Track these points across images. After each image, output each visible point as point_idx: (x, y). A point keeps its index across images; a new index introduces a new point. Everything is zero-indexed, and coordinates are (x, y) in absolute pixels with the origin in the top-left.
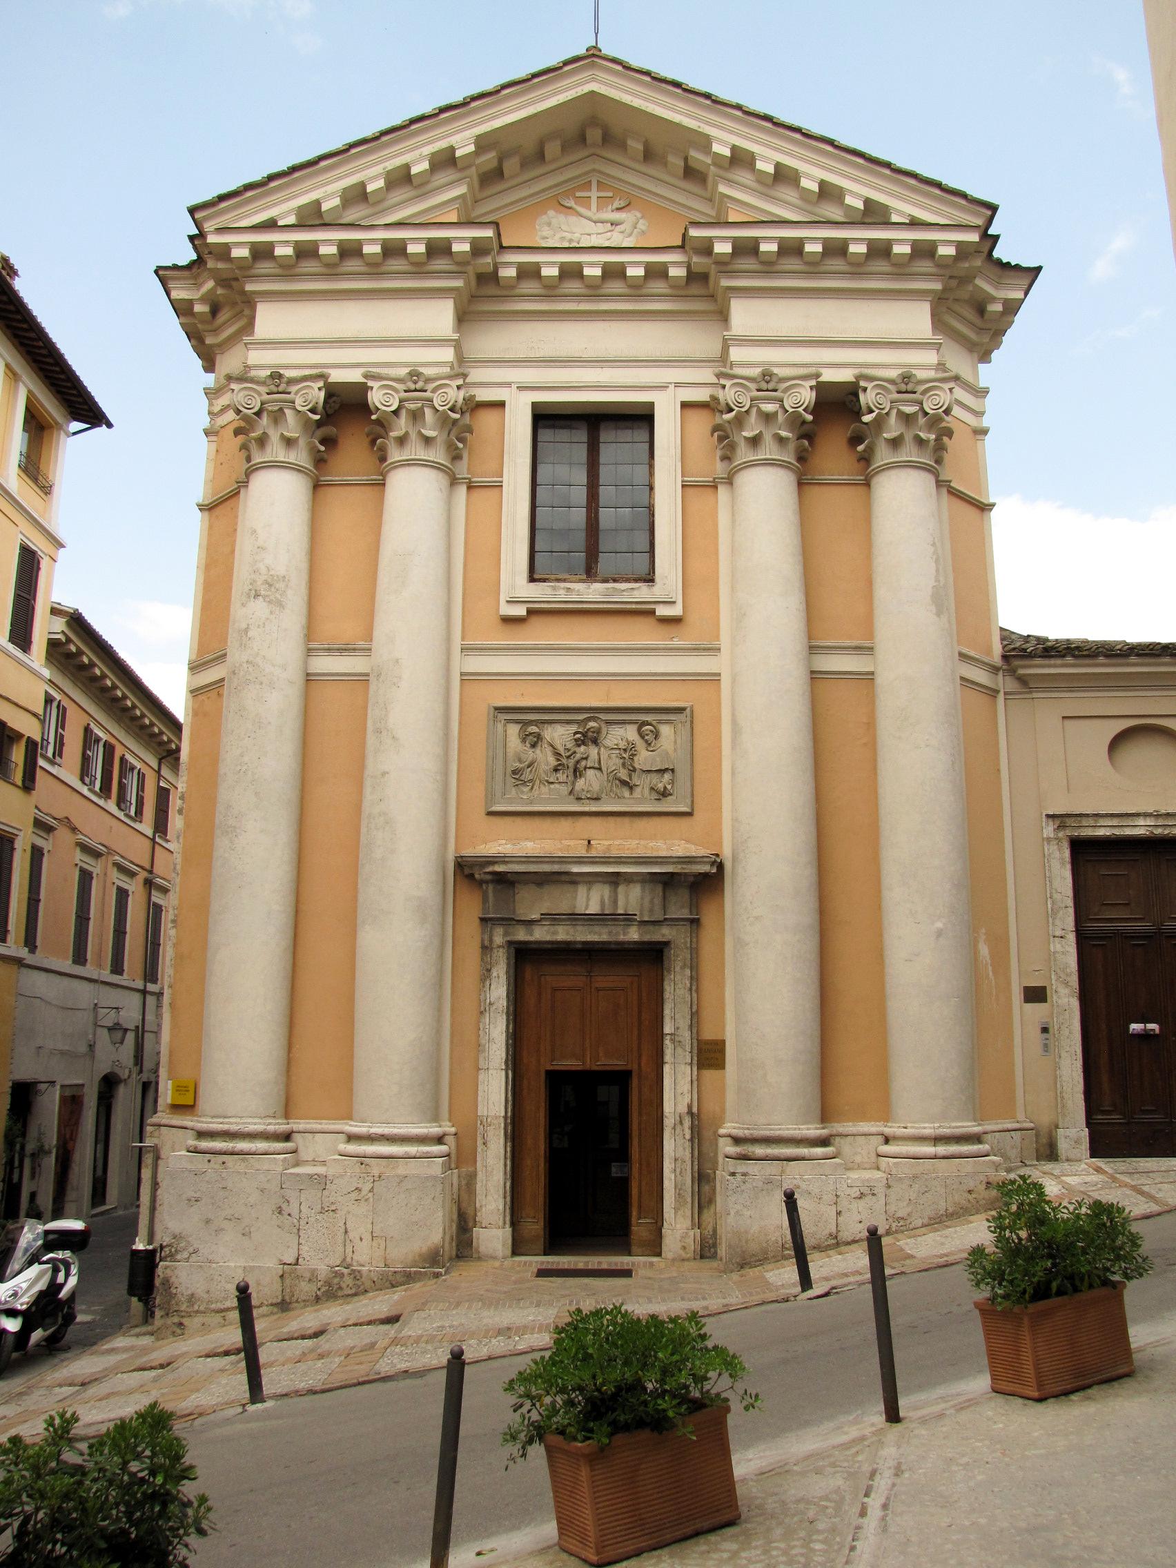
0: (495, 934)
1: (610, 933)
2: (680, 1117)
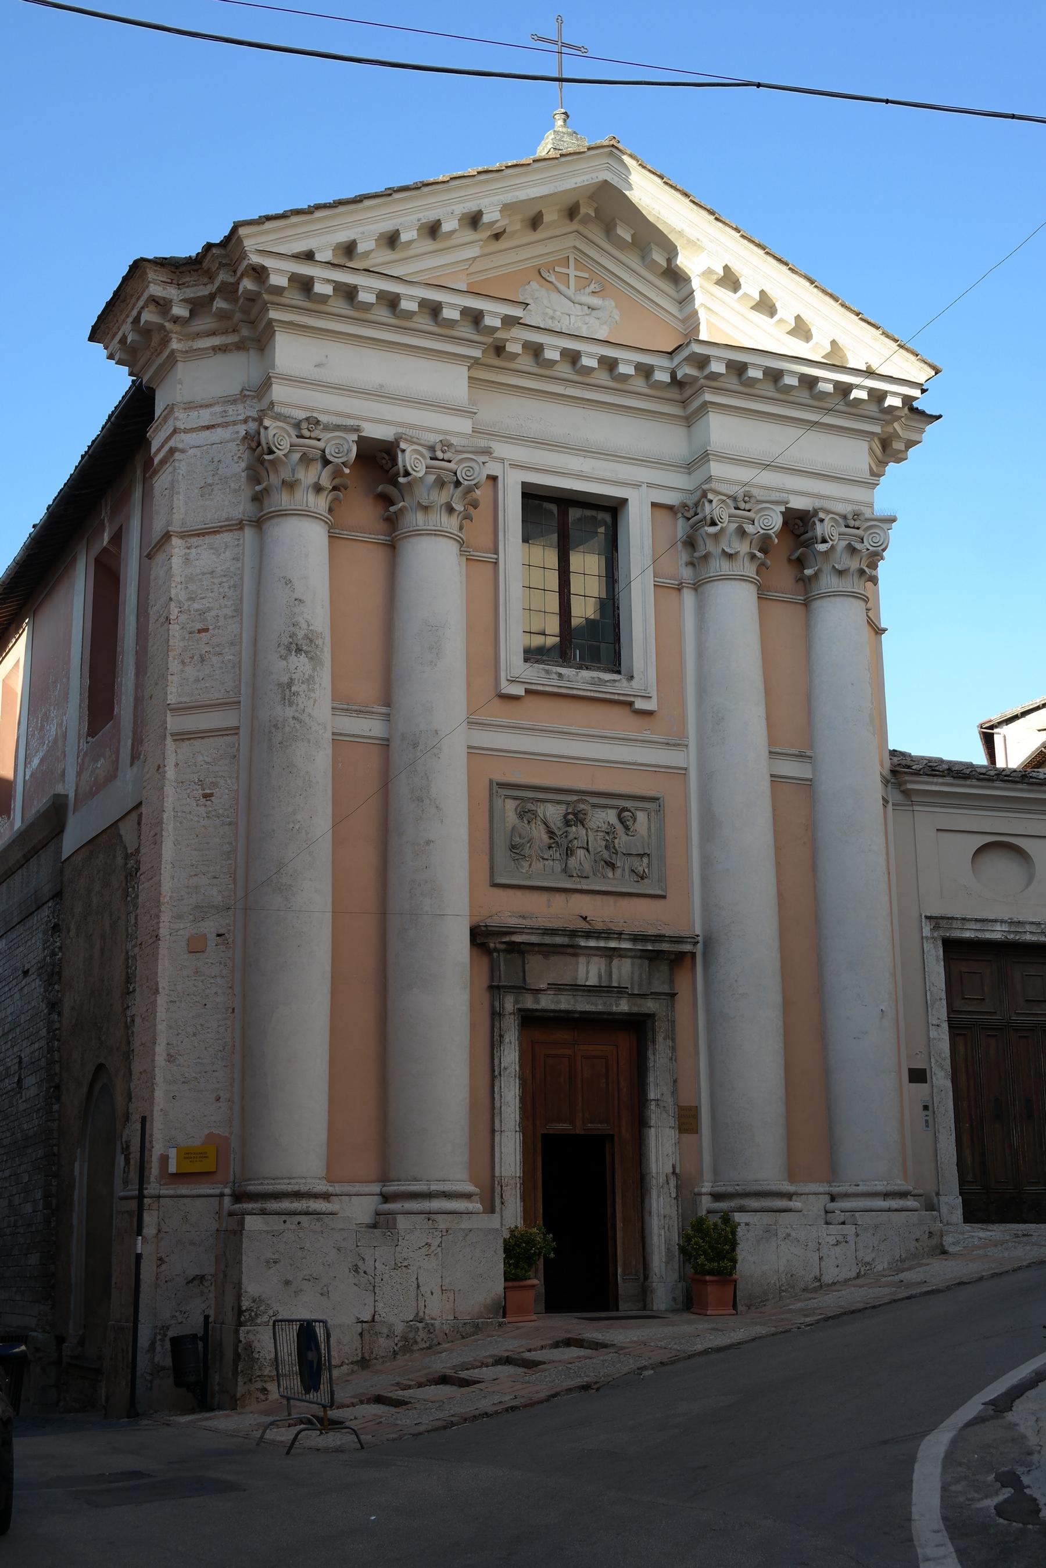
0: (506, 1001)
1: (605, 1004)
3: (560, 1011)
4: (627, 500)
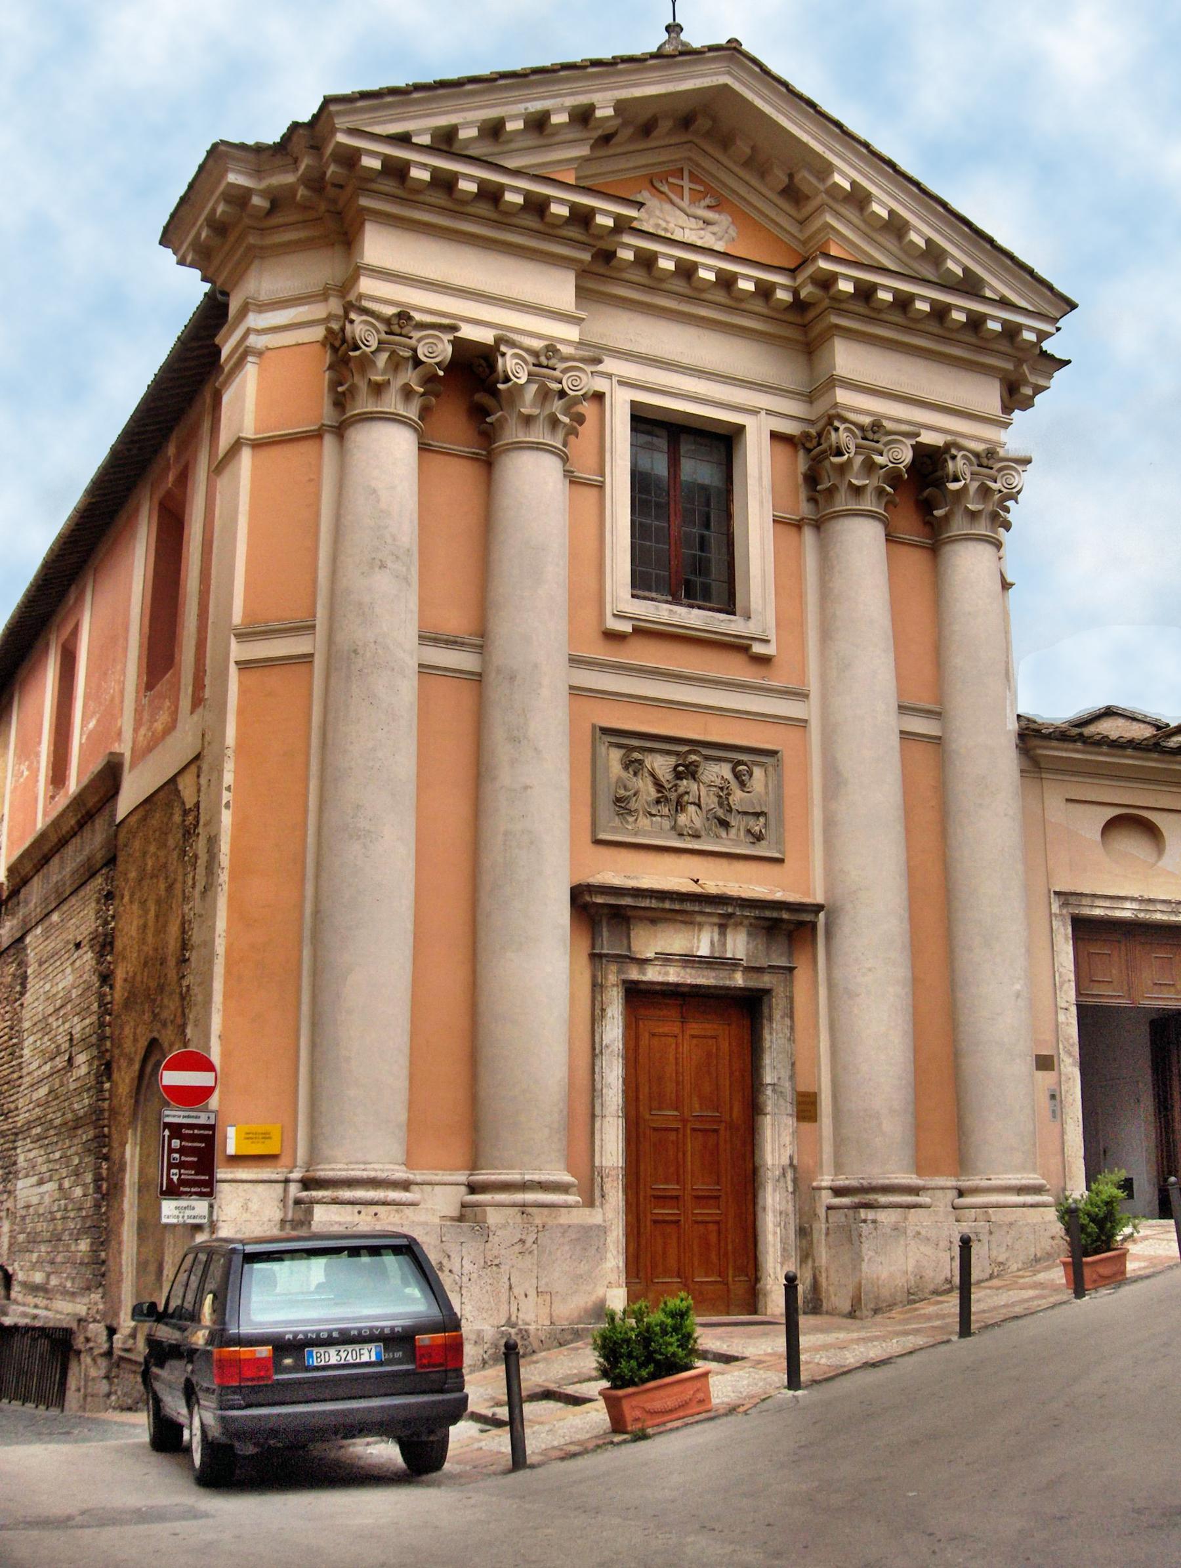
2: (783, 1169)
3: (668, 984)
4: (745, 426)
